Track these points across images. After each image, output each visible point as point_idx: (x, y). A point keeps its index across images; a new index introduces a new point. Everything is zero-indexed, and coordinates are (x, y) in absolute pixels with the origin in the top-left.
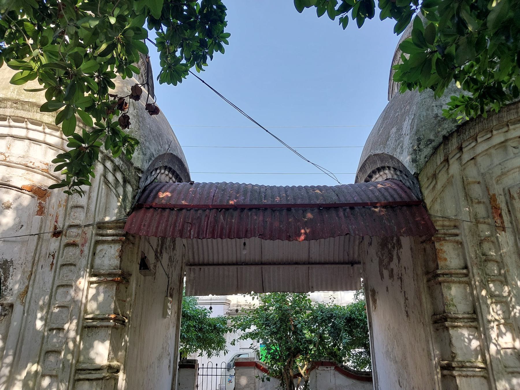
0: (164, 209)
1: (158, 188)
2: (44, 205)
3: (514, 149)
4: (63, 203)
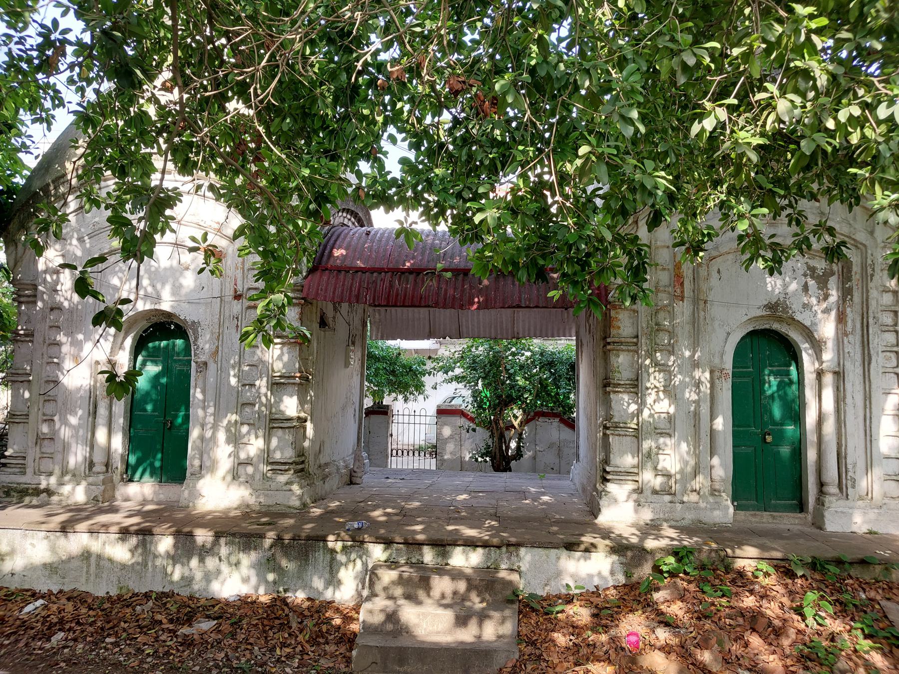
1: (332, 242)
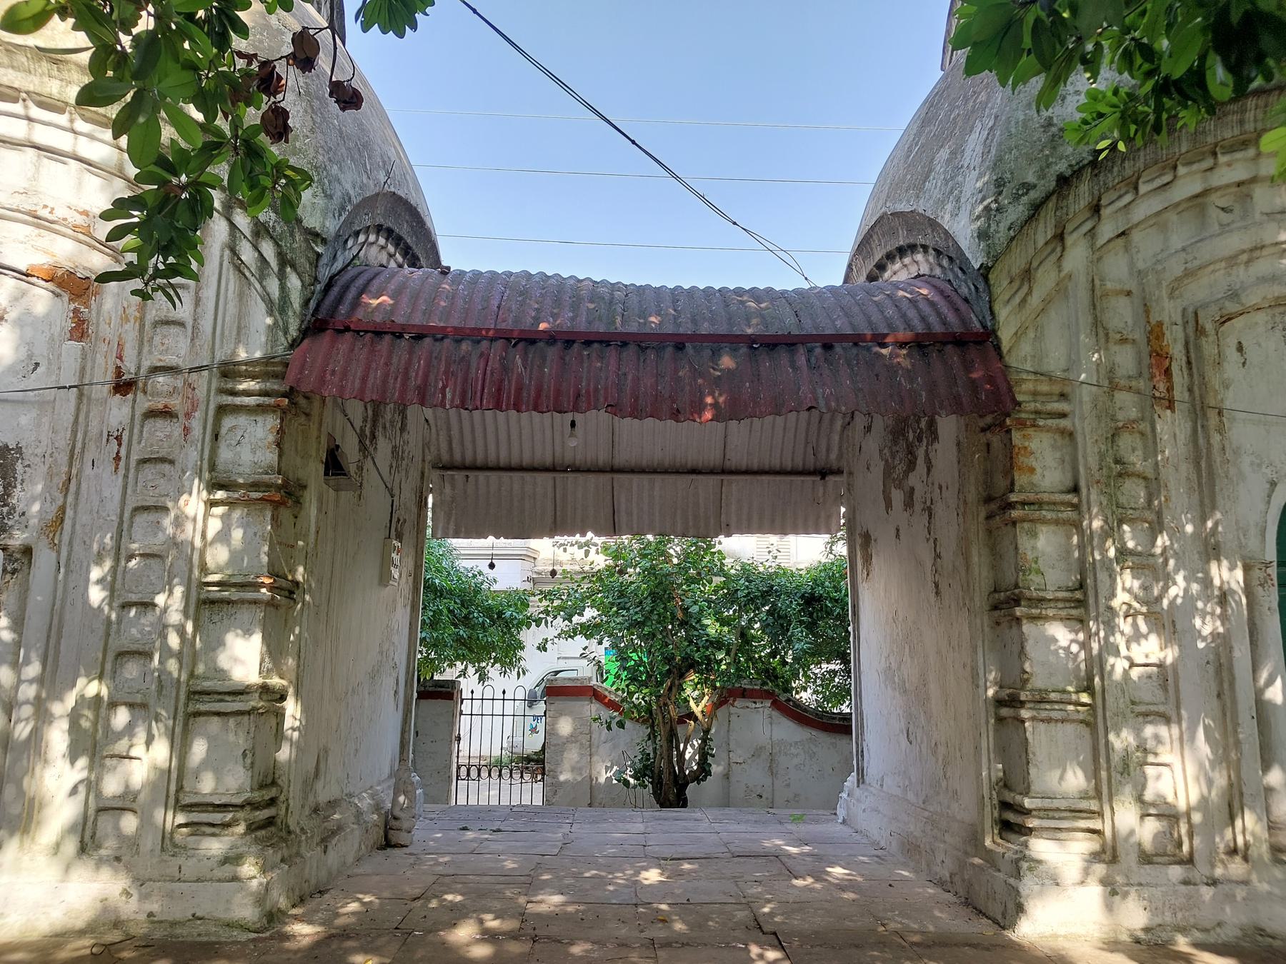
0: (378, 334)
1: (360, 282)
2: (85, 316)
3: (1222, 214)
4: (133, 312)
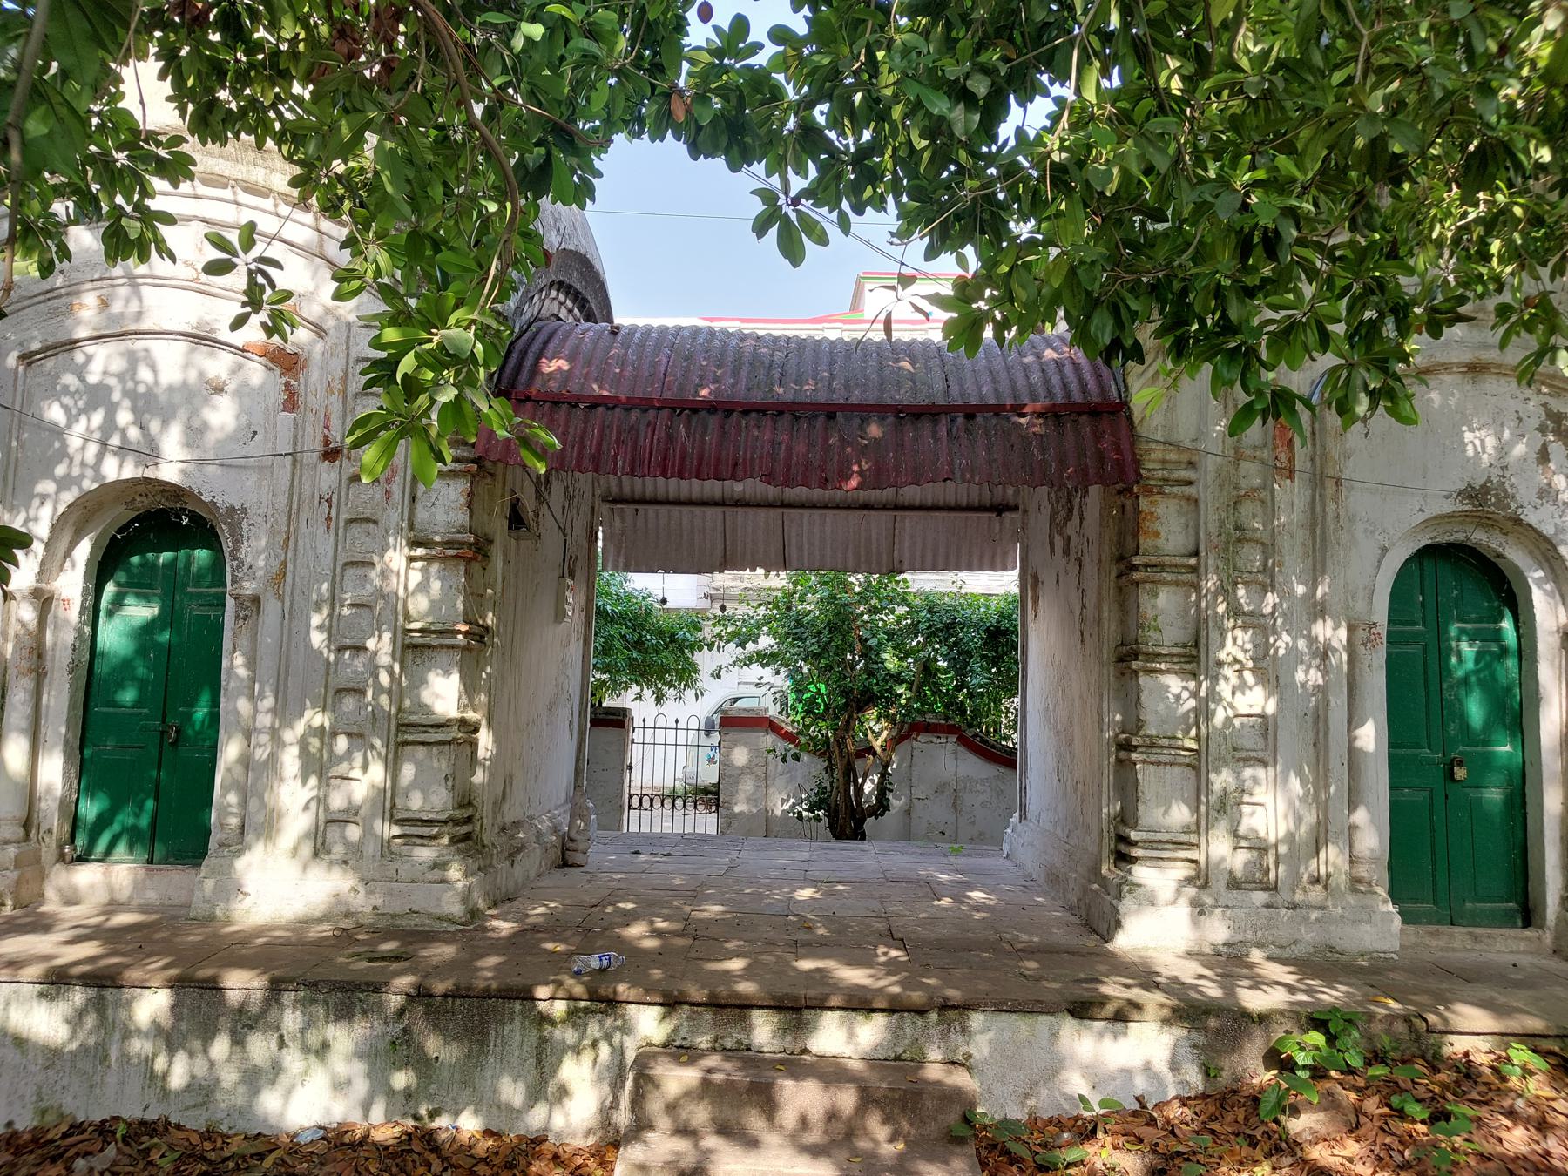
1: (536, 346)
2: (295, 389)
4: (337, 385)
